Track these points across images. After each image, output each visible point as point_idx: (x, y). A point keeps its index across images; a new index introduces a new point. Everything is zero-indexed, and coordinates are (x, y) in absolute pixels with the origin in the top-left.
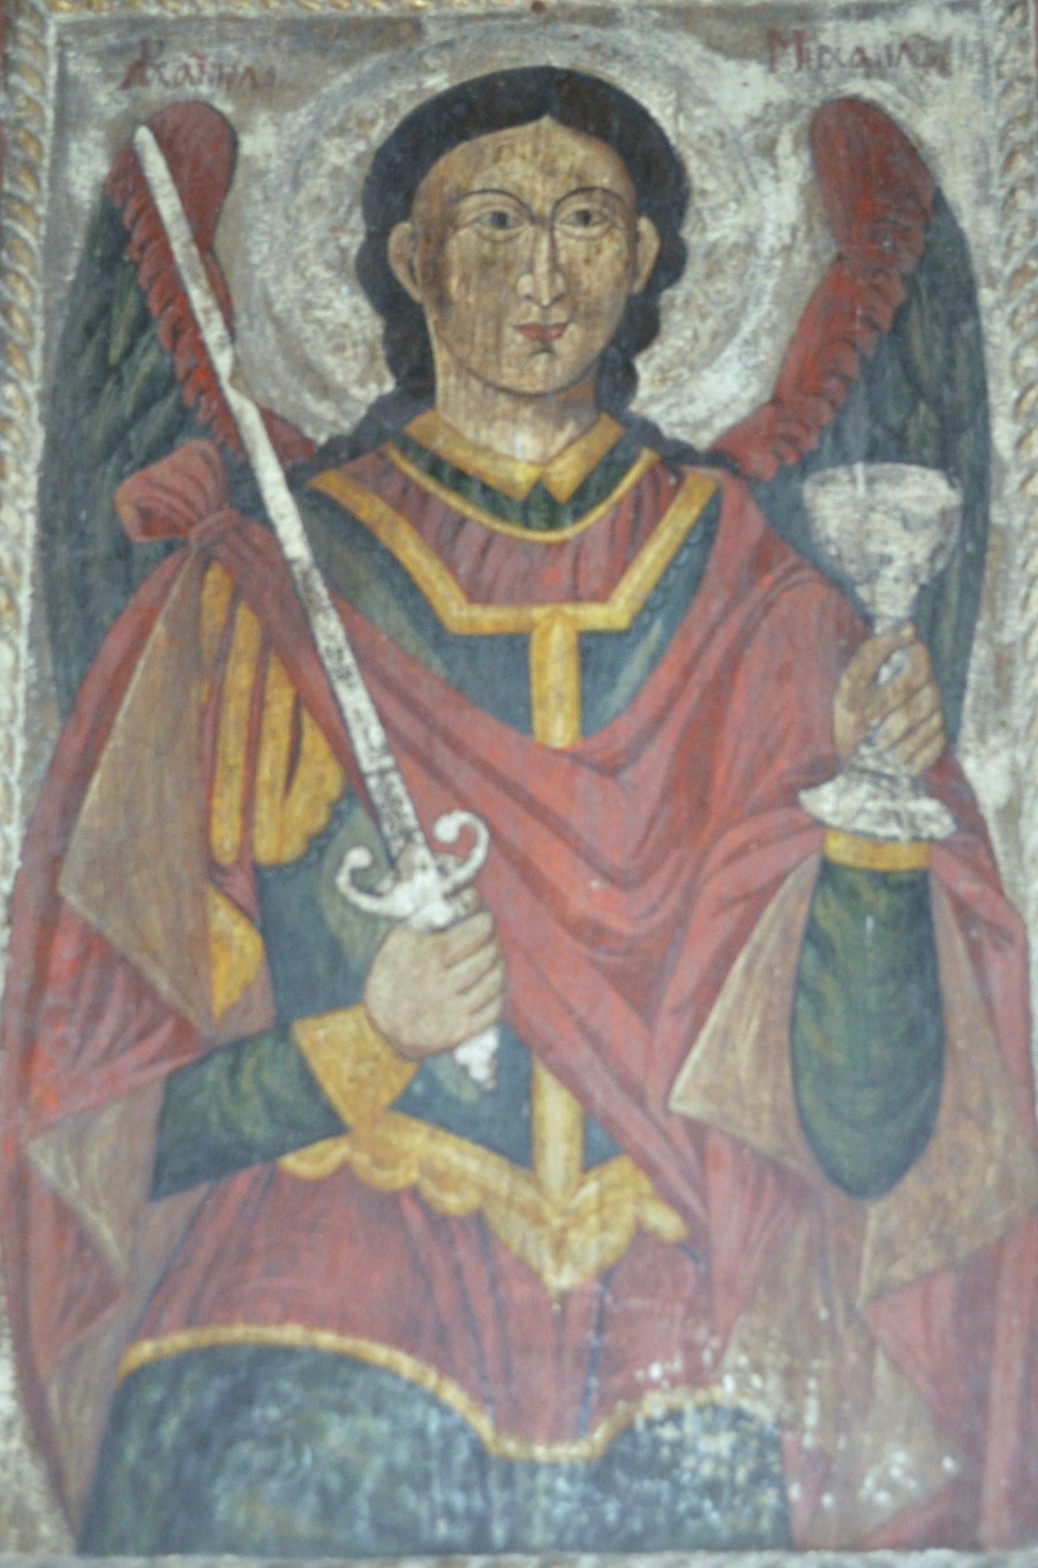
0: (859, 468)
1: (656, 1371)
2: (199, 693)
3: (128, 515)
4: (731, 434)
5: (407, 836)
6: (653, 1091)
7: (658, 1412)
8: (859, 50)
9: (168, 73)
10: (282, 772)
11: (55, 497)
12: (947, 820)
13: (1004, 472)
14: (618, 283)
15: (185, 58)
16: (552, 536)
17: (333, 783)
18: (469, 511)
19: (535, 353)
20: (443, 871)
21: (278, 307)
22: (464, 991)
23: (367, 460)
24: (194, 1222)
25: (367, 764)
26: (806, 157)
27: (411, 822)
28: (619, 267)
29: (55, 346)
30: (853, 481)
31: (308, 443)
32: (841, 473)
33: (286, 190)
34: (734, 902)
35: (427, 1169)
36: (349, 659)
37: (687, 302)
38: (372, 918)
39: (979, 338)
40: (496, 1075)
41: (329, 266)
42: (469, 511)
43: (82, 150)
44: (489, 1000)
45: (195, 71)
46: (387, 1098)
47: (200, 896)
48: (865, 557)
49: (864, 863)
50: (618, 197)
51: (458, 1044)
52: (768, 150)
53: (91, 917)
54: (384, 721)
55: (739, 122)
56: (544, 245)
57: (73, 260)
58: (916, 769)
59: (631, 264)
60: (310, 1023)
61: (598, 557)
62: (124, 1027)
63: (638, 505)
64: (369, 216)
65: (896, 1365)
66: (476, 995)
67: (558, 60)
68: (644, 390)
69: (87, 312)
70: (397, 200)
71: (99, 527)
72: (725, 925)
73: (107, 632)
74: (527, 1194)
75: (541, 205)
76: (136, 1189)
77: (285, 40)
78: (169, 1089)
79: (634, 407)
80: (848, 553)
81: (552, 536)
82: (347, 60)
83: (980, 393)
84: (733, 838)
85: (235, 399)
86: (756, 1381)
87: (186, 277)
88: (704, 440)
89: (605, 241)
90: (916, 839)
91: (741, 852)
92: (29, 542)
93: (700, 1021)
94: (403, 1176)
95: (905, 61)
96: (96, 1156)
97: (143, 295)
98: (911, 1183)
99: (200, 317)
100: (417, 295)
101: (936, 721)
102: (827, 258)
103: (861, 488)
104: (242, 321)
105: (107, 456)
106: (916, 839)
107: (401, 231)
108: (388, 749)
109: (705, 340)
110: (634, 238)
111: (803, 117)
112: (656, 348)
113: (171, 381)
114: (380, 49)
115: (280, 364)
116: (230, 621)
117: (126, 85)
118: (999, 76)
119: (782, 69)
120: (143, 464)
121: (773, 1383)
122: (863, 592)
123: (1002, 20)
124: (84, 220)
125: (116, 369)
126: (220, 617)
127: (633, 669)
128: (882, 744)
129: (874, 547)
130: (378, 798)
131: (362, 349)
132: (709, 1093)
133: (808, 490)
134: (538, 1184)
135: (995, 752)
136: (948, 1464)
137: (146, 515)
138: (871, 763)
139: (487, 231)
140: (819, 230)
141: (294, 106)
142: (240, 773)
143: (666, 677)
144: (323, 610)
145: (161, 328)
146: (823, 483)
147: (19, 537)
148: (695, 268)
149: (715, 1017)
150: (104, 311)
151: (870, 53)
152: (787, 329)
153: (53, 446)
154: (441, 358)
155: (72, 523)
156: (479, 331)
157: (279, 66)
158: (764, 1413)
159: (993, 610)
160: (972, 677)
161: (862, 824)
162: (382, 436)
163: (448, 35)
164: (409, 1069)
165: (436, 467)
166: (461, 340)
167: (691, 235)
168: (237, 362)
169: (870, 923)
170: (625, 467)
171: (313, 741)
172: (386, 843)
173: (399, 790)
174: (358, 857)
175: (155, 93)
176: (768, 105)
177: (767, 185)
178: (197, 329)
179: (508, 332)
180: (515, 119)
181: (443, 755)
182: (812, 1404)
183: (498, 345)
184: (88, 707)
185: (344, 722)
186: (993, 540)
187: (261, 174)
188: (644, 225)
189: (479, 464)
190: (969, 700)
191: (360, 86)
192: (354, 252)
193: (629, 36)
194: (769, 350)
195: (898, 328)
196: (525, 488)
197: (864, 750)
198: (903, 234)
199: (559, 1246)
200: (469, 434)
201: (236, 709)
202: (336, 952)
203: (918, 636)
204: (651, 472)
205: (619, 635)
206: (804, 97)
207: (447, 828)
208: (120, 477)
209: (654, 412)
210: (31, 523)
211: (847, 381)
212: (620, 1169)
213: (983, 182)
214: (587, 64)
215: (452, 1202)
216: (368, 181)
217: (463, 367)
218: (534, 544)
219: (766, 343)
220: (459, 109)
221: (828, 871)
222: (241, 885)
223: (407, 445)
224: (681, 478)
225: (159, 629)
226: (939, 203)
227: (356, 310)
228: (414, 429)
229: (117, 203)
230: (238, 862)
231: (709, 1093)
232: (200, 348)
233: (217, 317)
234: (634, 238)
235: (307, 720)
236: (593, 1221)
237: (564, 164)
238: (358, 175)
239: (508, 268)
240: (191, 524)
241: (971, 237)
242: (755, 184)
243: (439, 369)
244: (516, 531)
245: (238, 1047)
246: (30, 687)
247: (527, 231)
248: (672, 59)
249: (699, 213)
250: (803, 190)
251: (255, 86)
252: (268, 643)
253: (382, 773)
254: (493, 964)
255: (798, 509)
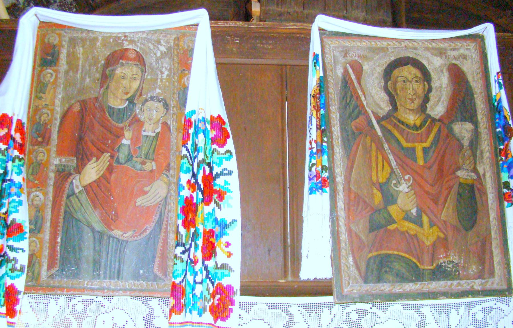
0: (460, 122)
1: (441, 256)
2: (368, 156)
3: (353, 127)
4: (441, 117)
5: (401, 178)
6: (439, 216)
7: (442, 262)
8: (454, 56)
9: (350, 55)
10: (381, 168)
11: (342, 124)
12: (476, 176)
13: (480, 123)
14: (423, 92)
15: (353, 53)
16: (418, 132)
17: (389, 171)
18: (405, 128)
19: (412, 103)
20: (406, 184)
21: (372, 94)
22: (411, 202)
23: (388, 120)
24: (376, 235)
25: (394, 168)
26: (448, 73)
27: (401, 176)
28: (422, 90)
29: (338, 100)
30: (459, 124)
31: (380, 117)
32: (457, 123)
33: (371, 75)
34: (448, 188)
35: (408, 228)
36: (389, 151)
37: (433, 96)
38: (397, 191)
39: (475, 103)
40: (417, 214)
41: (380, 88)
42: (405, 128)
43: (339, 68)
44: (414, 204)
45: (354, 55)
46: (401, 218)
47: (371, 188)
48: (461, 136)
49: (465, 183)
50: (421, 78)
51: (411, 210)
52: (442, 71)
53: (356, 191)
54: (396, 161)
55: (438, 67)
56: (411, 86)
57: (340, 86)
58: (471, 169)
59: (424, 89)
60: (390, 206)
61: (424, 136)
62: (362, 208)
63: (429, 128)
64: (384, 80)
65: (473, 254)
66: (413, 202)
67: (410, 55)
68: (428, 109)
69: (343, 94)
70: (388, 78)
71: (349, 129)
72: (447, 192)
73: (353, 146)
74: (422, 231)
75: (410, 79)
76: (367, 232)
77: (367, 50)
78: (370, 216)
79: (427, 112)
80: (459, 135)
81: (418, 132)
82: (378, 54)
83: (476, 111)
84: (447, 179)
85: (367, 109)
86: (455, 257)
87: (357, 89)
88: (437, 117)
89: (420, 85)
90: (472, 179)
91: (448, 181)
92: (339, 132)
93: (444, 206)
94: (405, 229)
95: (461, 58)
96: (361, 226)
97: (351, 92)
98: (474, 229)
99: (361, 96)
100: (393, 93)
101: (473, 161)
102: (452, 89)
103: (460, 126)
104: (367, 97)
105: (349, 118)
106: (472, 179)
107: (389, 82)
108: (397, 165)
109: (436, 101)
110: (424, 85)
111: (447, 67)
112: (430, 103)
113: (357, 106)
114: (382, 52)
115: (373, 104)
116: (371, 144)
117: (344, 57)
118: (474, 61)
119: (443, 58)
120: (355, 120)
121: (457, 258)
122: (462, 142)
123: (474, 52)
124: (340, 79)
125: (349, 104)
126: (369, 144)
127: (431, 153)
128: (466, 165)
129: (463, 135)
130: (396, 173)
131: (386, 102)
132: (446, 216)
133: (453, 126)
134: (424, 230)
135: (481, 166)
136: (480, 268)
137: (356, 128)
138: (465, 168)
139: (402, 83)
140: (451, 84)
141: (370, 61)
142: (375, 169)
143: (436, 154)
144: (384, 143)
145: (355, 97)
146: (455, 124)
147: (338, 131)
148: (434, 90)
149: (446, 206)
150: (346, 93)
151: (455, 56)
152: (448, 100)
153: (341, 117)
154: (398, 103)
155: (345, 129)
156: (403, 99)
157: (367, 55)
158: (456, 261)
159: (480, 145)
160: (478, 155)
161: (464, 177)
162: (391, 116)
163: (393, 50)
164: (404, 213)
165: (399, 121)
166: (401, 101)
167: (433, 85)
168: (367, 103)
169: (466, 191)
170: (426, 122)
171: (385, 163)
172: (398, 179)
173: (399, 171)
174: (394, 182)
175: (349, 59)
176: (441, 64)
177: (442, 77)
178: (360, 98)
179: (407, 99)
180: (405, 65)
181: (405, 166)
182: (462, 260)
183: (406, 102)
184: (351, 158)
185: (390, 161)
186: (479, 134)
187: (367, 72)
188: (425, 83)
189: (405, 120)
190: (477, 158)
191: (380, 58)
192: (383, 86)
193: (420, 52)
194: (446, 103)
195: (463, 101)
196: (412, 125)
197: (464, 166)
198: (463, 86)
199: (427, 239)
200: (403, 116)
201: (373, 159)
202: (392, 196)
203: (470, 149)
204: (430, 123)
205: (429, 148)
206: (446, 63)
207: (407, 177)
208: (352, 122)
209: (430, 113)
210: (339, 128)
211: (457, 109)
212: (435, 228)
213: (473, 78)
214: (414, 56)
215: (412, 233)
216: (383, 74)
217: (401, 105)
218: (414, 133)
219: (445, 102)
220: (396, 63)
221: (460, 184)
222: (377, 185)
223: (394, 117)
224: (435, 123)
225: (360, 146)
226: (467, 82)
227: (384, 96)
228: (395, 115)
229: (345, 76)
230: (377, 182)
231: (446, 216)
232: (361, 100)
233: (363, 96)
234: (424, 85)
235: (384, 161)
236: (432, 235)
237: (413, 73)
238: (382, 73)
239: (406, 89)
240: (363, 129)
241: (473, 87)
242: (441, 77)
243: (398, 105)
244: (412, 131)
245: (380, 210)
246: (342, 155)
247: (408, 83)
248: (426, 56)
249: (433, 81)
250: (448, 78)
251: (364, 58)
252: (377, 148)
253: (396, 169)
254: (415, 198)
255: (452, 128)
